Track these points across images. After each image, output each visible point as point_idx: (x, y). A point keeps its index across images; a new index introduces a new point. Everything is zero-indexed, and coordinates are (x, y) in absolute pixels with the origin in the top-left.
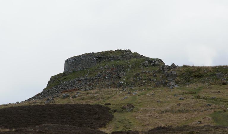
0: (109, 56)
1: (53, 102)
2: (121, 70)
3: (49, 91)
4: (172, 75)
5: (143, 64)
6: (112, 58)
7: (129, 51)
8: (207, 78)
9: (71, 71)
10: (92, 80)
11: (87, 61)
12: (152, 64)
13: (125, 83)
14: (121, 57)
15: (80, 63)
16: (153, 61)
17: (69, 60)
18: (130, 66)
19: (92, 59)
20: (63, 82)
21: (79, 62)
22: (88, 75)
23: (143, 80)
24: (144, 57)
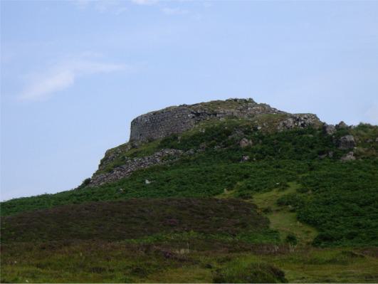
5: (284, 123)
12: (300, 123)
14: (238, 113)
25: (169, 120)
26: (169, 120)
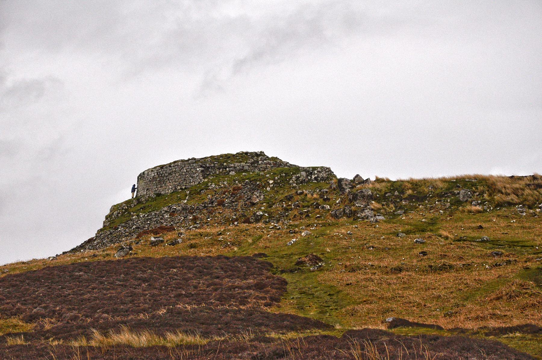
0: (225, 164)
1: (131, 254)
2: (253, 189)
3: (111, 234)
4: (363, 197)
5: (296, 177)
6: (231, 167)
7: (262, 154)
8: (438, 201)
9: (152, 195)
10: (196, 209)
11: (184, 174)
12: (313, 177)
13: (266, 215)
14: (249, 166)
15: (168, 179)
16: (316, 172)
17: (146, 173)
18: (271, 182)
19: (192, 170)
20: (138, 216)
21: (167, 176)
22: (188, 200)
23: (304, 207)
24: (291, 165)
25: (177, 175)
26: (177, 175)
